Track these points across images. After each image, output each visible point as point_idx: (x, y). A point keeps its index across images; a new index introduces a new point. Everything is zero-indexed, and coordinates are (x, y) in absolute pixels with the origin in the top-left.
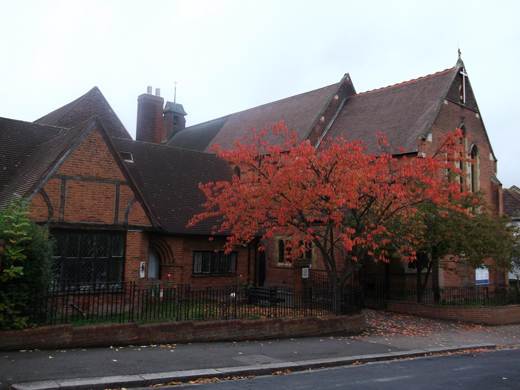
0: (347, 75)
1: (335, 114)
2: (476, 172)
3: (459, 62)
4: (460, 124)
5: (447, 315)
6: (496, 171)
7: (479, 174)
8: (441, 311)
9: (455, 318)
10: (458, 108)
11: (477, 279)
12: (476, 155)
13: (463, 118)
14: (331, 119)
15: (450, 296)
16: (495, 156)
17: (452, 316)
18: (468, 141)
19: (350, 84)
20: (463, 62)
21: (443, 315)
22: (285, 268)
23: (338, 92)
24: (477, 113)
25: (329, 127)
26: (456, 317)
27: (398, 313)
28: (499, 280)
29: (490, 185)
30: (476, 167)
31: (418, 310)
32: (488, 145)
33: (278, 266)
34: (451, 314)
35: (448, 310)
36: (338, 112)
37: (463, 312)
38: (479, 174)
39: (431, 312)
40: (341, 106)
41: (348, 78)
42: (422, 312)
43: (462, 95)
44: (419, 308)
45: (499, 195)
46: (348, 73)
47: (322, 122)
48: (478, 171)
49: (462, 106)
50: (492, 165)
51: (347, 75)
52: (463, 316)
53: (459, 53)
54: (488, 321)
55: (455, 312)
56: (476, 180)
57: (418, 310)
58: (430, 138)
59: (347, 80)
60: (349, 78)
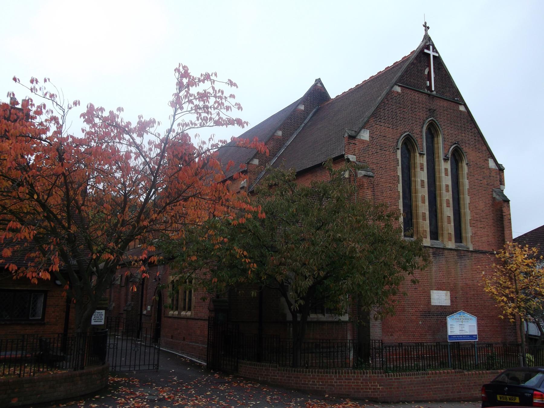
0: (318, 81)
1: (299, 127)
2: (440, 177)
3: (424, 39)
4: (427, 118)
5: (307, 384)
6: (502, 182)
7: (467, 187)
8: (299, 378)
9: (320, 389)
10: (424, 98)
11: (449, 333)
12: (461, 160)
13: (432, 112)
14: (291, 134)
15: (411, 357)
16: (499, 163)
17: (316, 385)
18: (444, 140)
19: (324, 91)
20: (430, 38)
21: (303, 384)
22: (174, 318)
23: (304, 102)
24: (461, 104)
25: (288, 143)
26: (321, 388)
27: (247, 379)
28: (509, 337)
29: (491, 202)
30: (463, 177)
31: (269, 375)
32: (484, 148)
33: (170, 315)
34: (314, 382)
35: (327, 376)
36: (303, 125)
37: (333, 379)
38: (467, 187)
39: (285, 378)
40: (308, 118)
41: (319, 85)
42: (273, 378)
43: (430, 81)
44: (271, 373)
45: (502, 215)
46: (320, 79)
47: (279, 137)
48: (465, 183)
49: (429, 95)
50: (493, 174)
51: (318, 81)
52: (333, 386)
53: (427, 28)
54: (379, 395)
55: (319, 379)
56: (463, 194)
57: (269, 375)
58: (365, 135)
59: (317, 86)
60: (322, 84)
